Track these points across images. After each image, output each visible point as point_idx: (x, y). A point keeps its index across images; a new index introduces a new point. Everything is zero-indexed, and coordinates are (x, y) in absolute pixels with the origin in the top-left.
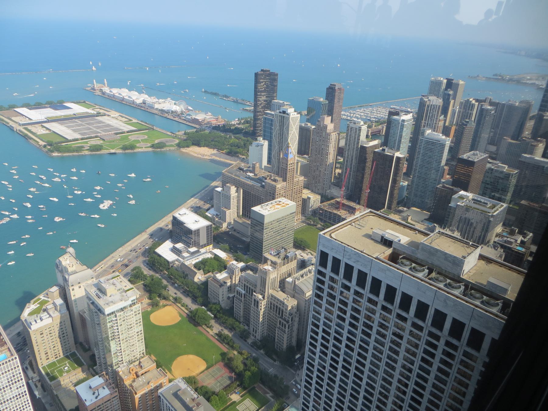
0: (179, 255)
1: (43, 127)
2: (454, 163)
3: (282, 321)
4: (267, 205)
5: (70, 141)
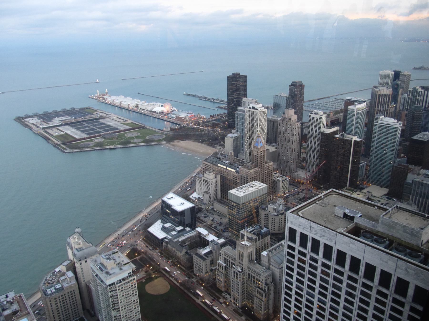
0: (167, 233)
1: (58, 129)
2: (407, 143)
3: (260, 290)
5: (79, 140)
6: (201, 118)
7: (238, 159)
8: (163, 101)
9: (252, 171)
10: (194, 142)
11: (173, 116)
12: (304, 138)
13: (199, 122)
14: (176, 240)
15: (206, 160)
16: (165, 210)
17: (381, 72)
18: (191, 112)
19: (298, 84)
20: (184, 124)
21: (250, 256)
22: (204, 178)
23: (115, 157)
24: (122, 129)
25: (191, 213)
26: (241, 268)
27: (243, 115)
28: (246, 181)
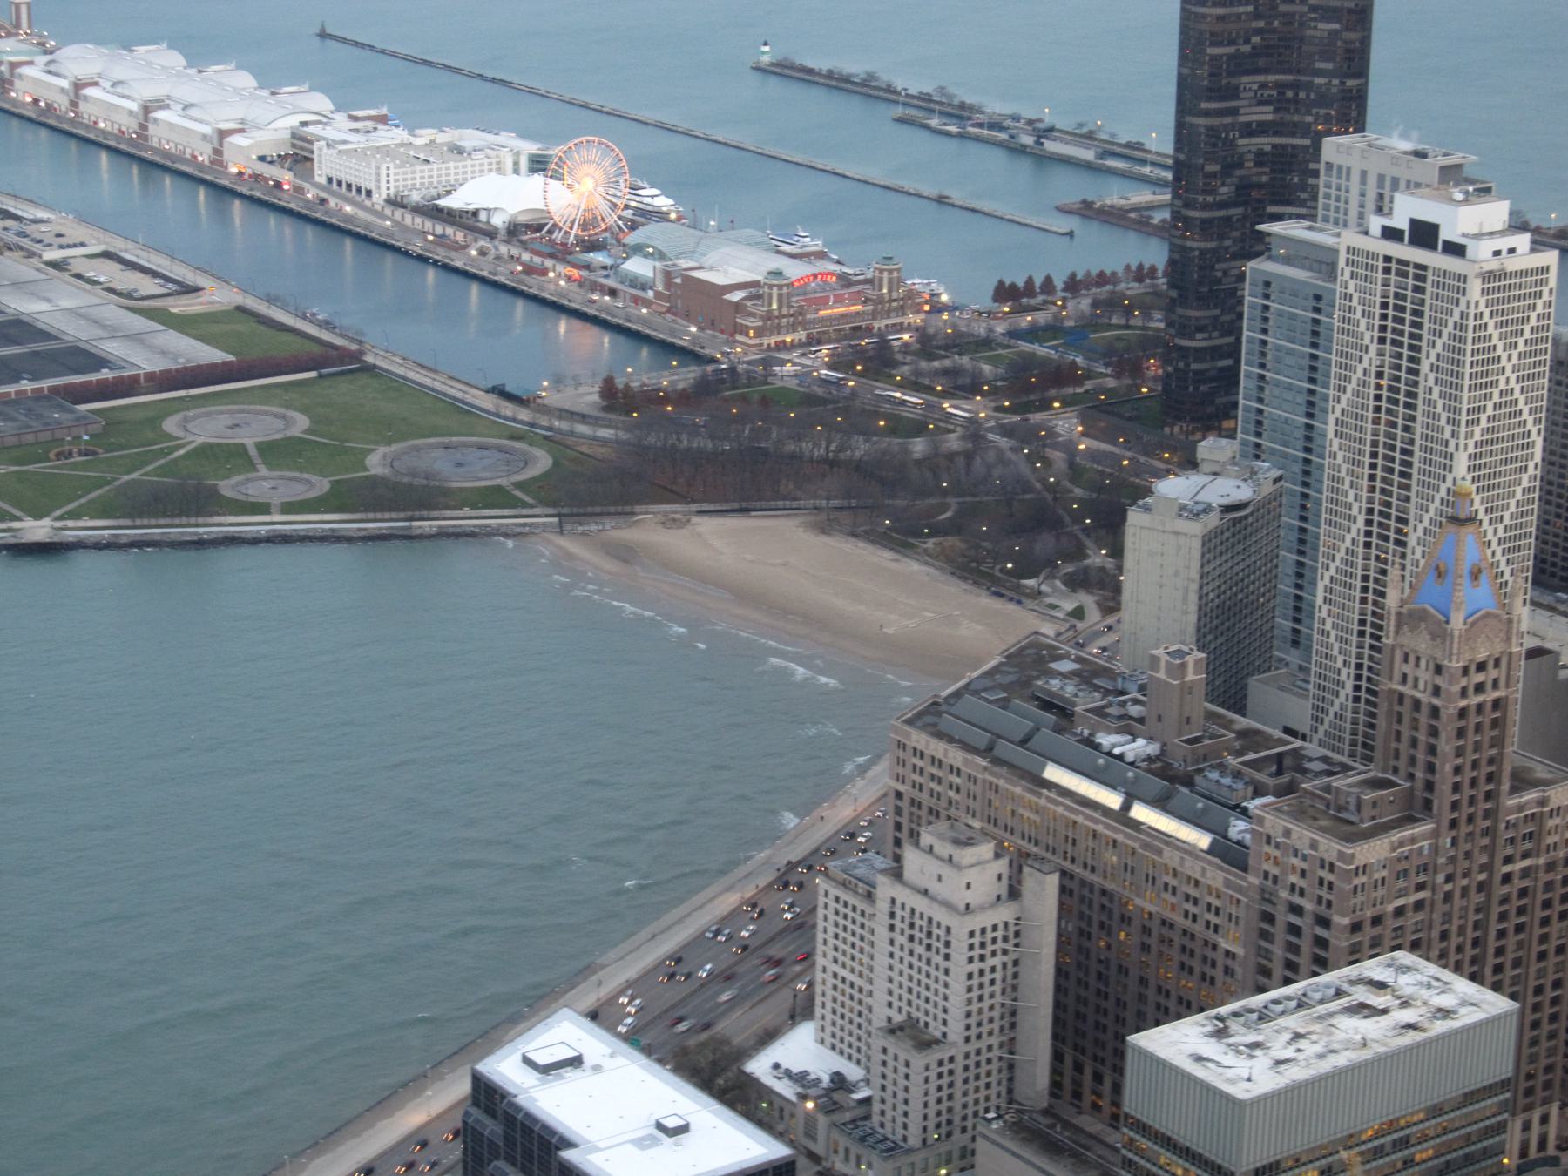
4: (1263, 1017)
6: (909, 301)
7: (1243, 722)
8: (553, 117)
9: (1374, 851)
10: (823, 529)
11: (638, 266)
13: (884, 345)
15: (930, 717)
18: (815, 245)
20: (742, 351)
22: (902, 894)
24: (144, 362)
27: (1318, 301)
28: (1306, 945)
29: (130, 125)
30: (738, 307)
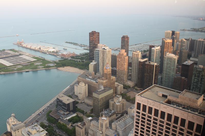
11: (60, 53)
12: (130, 65)
14: (65, 119)
15: (79, 76)
16: (59, 104)
17: (166, 32)
19: (126, 37)
20: (67, 58)
21: (106, 125)
23: (28, 75)
25: (73, 105)
26: (102, 132)
29: (30, 47)
30: (66, 55)
